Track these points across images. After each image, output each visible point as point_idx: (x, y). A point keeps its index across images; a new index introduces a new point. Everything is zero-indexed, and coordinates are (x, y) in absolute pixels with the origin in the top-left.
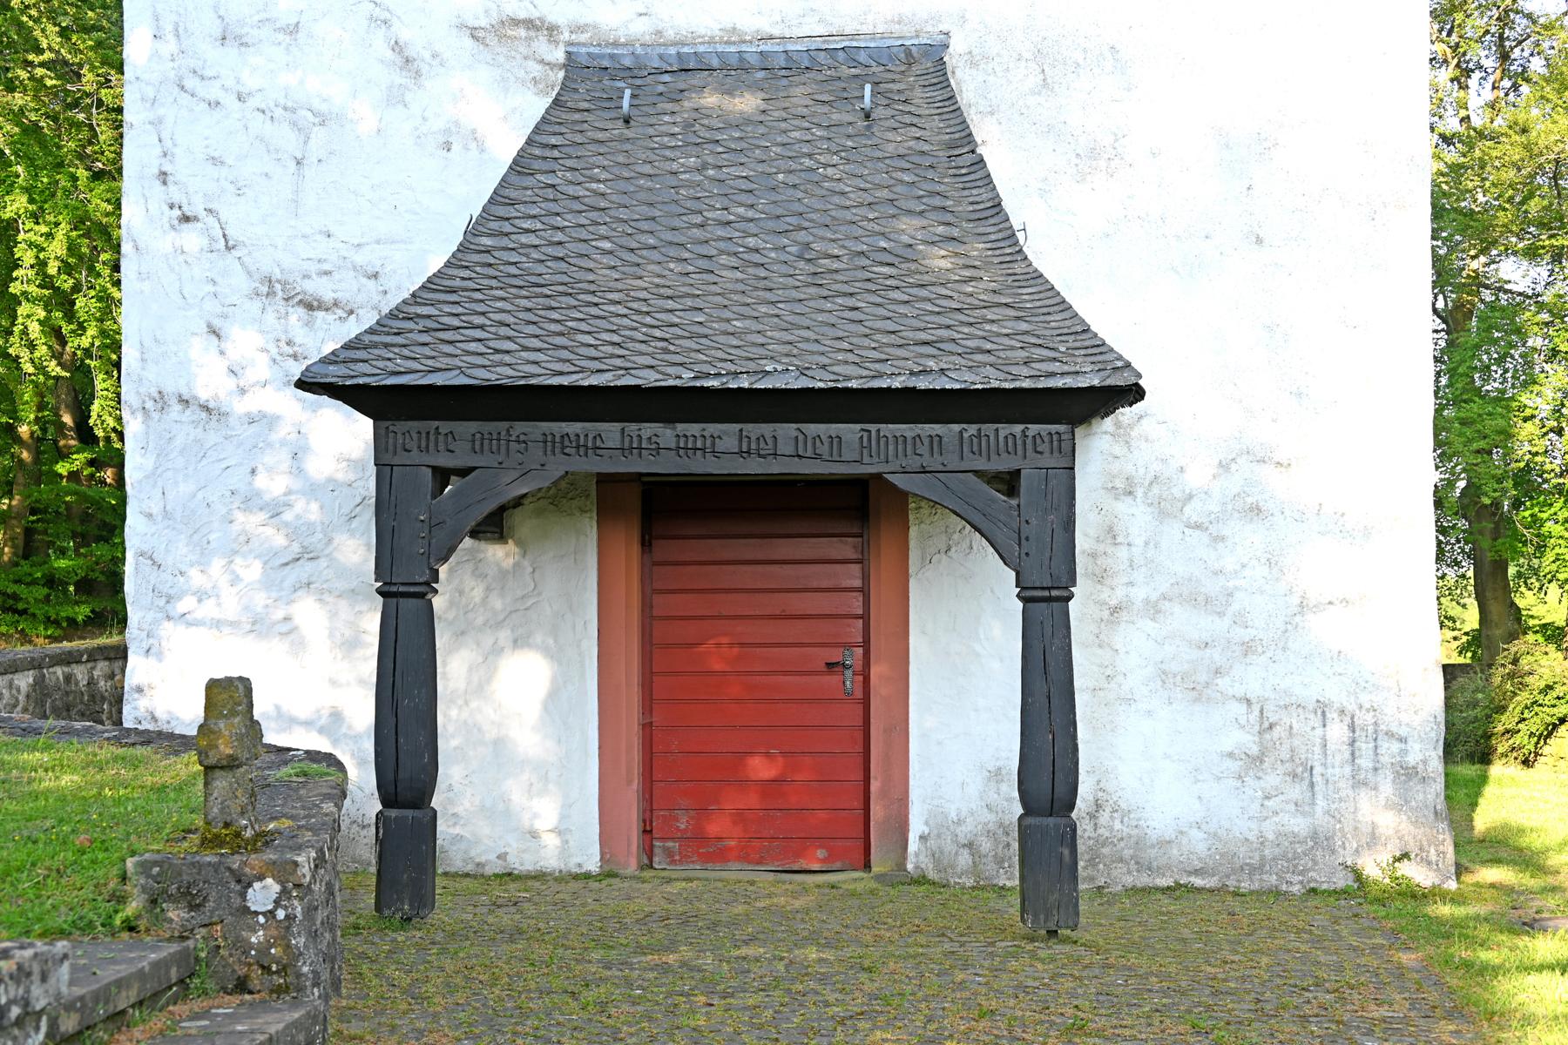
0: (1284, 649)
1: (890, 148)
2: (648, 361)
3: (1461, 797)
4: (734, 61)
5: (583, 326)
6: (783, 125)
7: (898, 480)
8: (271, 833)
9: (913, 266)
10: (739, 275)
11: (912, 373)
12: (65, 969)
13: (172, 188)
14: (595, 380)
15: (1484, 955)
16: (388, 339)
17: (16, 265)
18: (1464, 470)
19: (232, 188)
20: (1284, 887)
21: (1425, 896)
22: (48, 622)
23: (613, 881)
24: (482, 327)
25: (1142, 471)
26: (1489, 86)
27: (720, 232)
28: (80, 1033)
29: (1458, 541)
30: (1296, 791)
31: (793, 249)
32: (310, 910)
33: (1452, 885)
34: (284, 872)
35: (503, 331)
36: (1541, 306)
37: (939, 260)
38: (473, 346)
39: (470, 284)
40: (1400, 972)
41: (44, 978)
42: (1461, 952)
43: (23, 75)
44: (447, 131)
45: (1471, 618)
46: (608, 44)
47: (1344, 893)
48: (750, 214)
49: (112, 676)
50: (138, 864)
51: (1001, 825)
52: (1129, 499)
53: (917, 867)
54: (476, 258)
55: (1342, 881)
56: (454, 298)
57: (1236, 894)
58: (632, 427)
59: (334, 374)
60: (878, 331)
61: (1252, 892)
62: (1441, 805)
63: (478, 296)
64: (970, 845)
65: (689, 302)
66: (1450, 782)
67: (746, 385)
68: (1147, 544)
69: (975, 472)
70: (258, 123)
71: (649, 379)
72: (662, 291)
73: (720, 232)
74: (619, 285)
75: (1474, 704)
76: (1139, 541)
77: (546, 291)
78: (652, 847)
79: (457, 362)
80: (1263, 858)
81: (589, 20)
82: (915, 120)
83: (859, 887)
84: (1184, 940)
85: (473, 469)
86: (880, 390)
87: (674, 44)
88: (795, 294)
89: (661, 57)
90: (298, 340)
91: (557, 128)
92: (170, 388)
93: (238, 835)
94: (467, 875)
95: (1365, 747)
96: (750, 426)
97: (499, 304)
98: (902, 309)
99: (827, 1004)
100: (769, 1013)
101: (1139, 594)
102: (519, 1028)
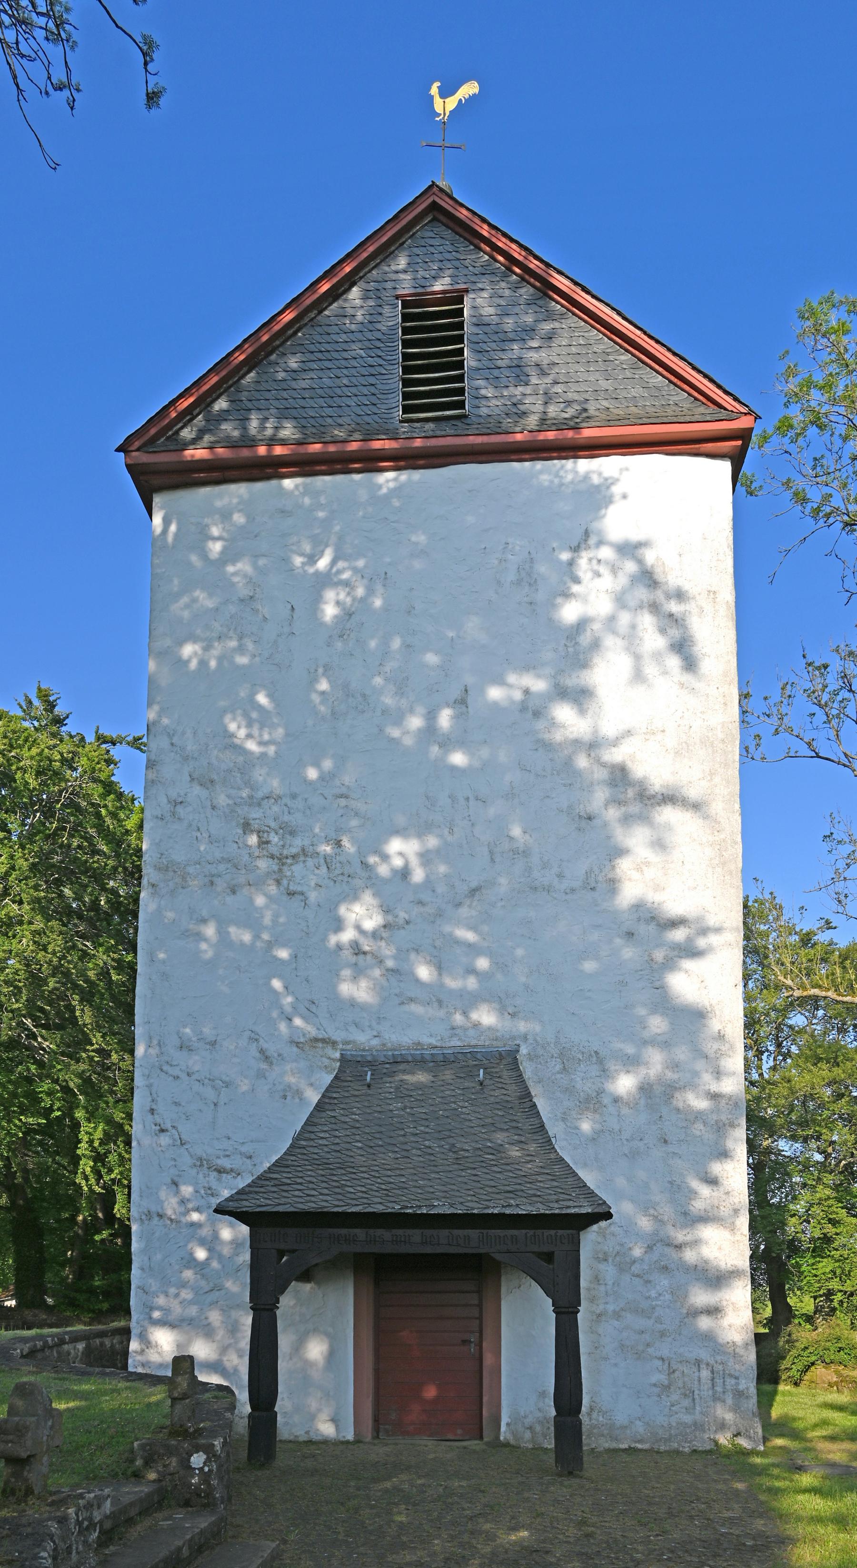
0: (680, 1334)
1: (492, 1099)
2: (379, 1200)
3: (766, 1400)
4: (419, 1058)
5: (349, 1183)
6: (442, 1088)
7: (498, 1257)
8: (202, 1429)
9: (503, 1155)
10: (422, 1159)
11: (503, 1206)
12: (109, 1502)
13: (156, 1116)
14: (354, 1209)
15: (778, 1484)
16: (257, 1189)
17: (80, 1142)
18: (763, 1241)
19: (184, 1117)
20: (681, 1449)
21: (748, 1454)
22: (90, 1311)
23: (361, 1445)
24: (301, 1184)
25: (611, 1249)
26: (772, 1059)
27: (413, 1139)
28: (112, 1529)
29: (761, 1274)
30: (686, 1403)
31: (447, 1147)
32: (219, 1467)
33: (761, 1448)
34: (208, 1449)
35: (311, 1186)
36: (799, 1163)
37: (515, 1152)
38: (297, 1193)
39: (296, 1163)
40: (737, 1493)
41: (99, 1507)
42: (766, 1482)
43: (84, 1055)
44: (285, 1090)
45: (768, 1312)
46: (360, 1050)
47: (710, 1452)
48: (427, 1130)
49: (122, 1342)
50: (138, 1445)
51: (545, 1418)
52: (605, 1263)
53: (505, 1438)
54: (298, 1151)
55: (708, 1446)
56: (286, 1170)
57: (658, 1452)
58: (371, 1231)
59: (232, 1205)
60: (487, 1186)
61: (665, 1451)
62: (755, 1409)
63: (300, 1169)
64: (530, 1428)
65: (398, 1172)
66: (760, 1393)
67: (425, 1212)
68: (614, 1284)
69: (533, 1253)
70: (197, 1087)
71: (379, 1208)
72: (385, 1167)
73: (413, 1139)
74: (366, 1164)
75: (770, 1355)
76: (610, 1283)
77: (331, 1167)
78: (379, 1428)
79: (289, 1200)
80: (670, 1435)
81: (352, 1039)
82: (504, 1086)
83: (477, 1448)
84: (633, 1477)
85: (296, 1250)
86: (488, 1214)
87: (391, 1050)
88: (447, 1168)
89: (385, 1056)
90: (214, 1187)
91: (336, 1090)
92: (153, 1209)
93: (186, 1431)
94: (290, 1441)
95: (719, 1381)
96: (426, 1231)
97: (309, 1173)
98: (498, 1176)
99: (464, 1509)
100: (436, 1514)
101: (611, 1308)
102: (317, 1521)
